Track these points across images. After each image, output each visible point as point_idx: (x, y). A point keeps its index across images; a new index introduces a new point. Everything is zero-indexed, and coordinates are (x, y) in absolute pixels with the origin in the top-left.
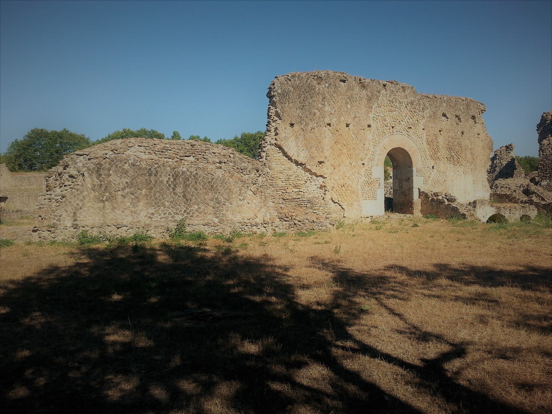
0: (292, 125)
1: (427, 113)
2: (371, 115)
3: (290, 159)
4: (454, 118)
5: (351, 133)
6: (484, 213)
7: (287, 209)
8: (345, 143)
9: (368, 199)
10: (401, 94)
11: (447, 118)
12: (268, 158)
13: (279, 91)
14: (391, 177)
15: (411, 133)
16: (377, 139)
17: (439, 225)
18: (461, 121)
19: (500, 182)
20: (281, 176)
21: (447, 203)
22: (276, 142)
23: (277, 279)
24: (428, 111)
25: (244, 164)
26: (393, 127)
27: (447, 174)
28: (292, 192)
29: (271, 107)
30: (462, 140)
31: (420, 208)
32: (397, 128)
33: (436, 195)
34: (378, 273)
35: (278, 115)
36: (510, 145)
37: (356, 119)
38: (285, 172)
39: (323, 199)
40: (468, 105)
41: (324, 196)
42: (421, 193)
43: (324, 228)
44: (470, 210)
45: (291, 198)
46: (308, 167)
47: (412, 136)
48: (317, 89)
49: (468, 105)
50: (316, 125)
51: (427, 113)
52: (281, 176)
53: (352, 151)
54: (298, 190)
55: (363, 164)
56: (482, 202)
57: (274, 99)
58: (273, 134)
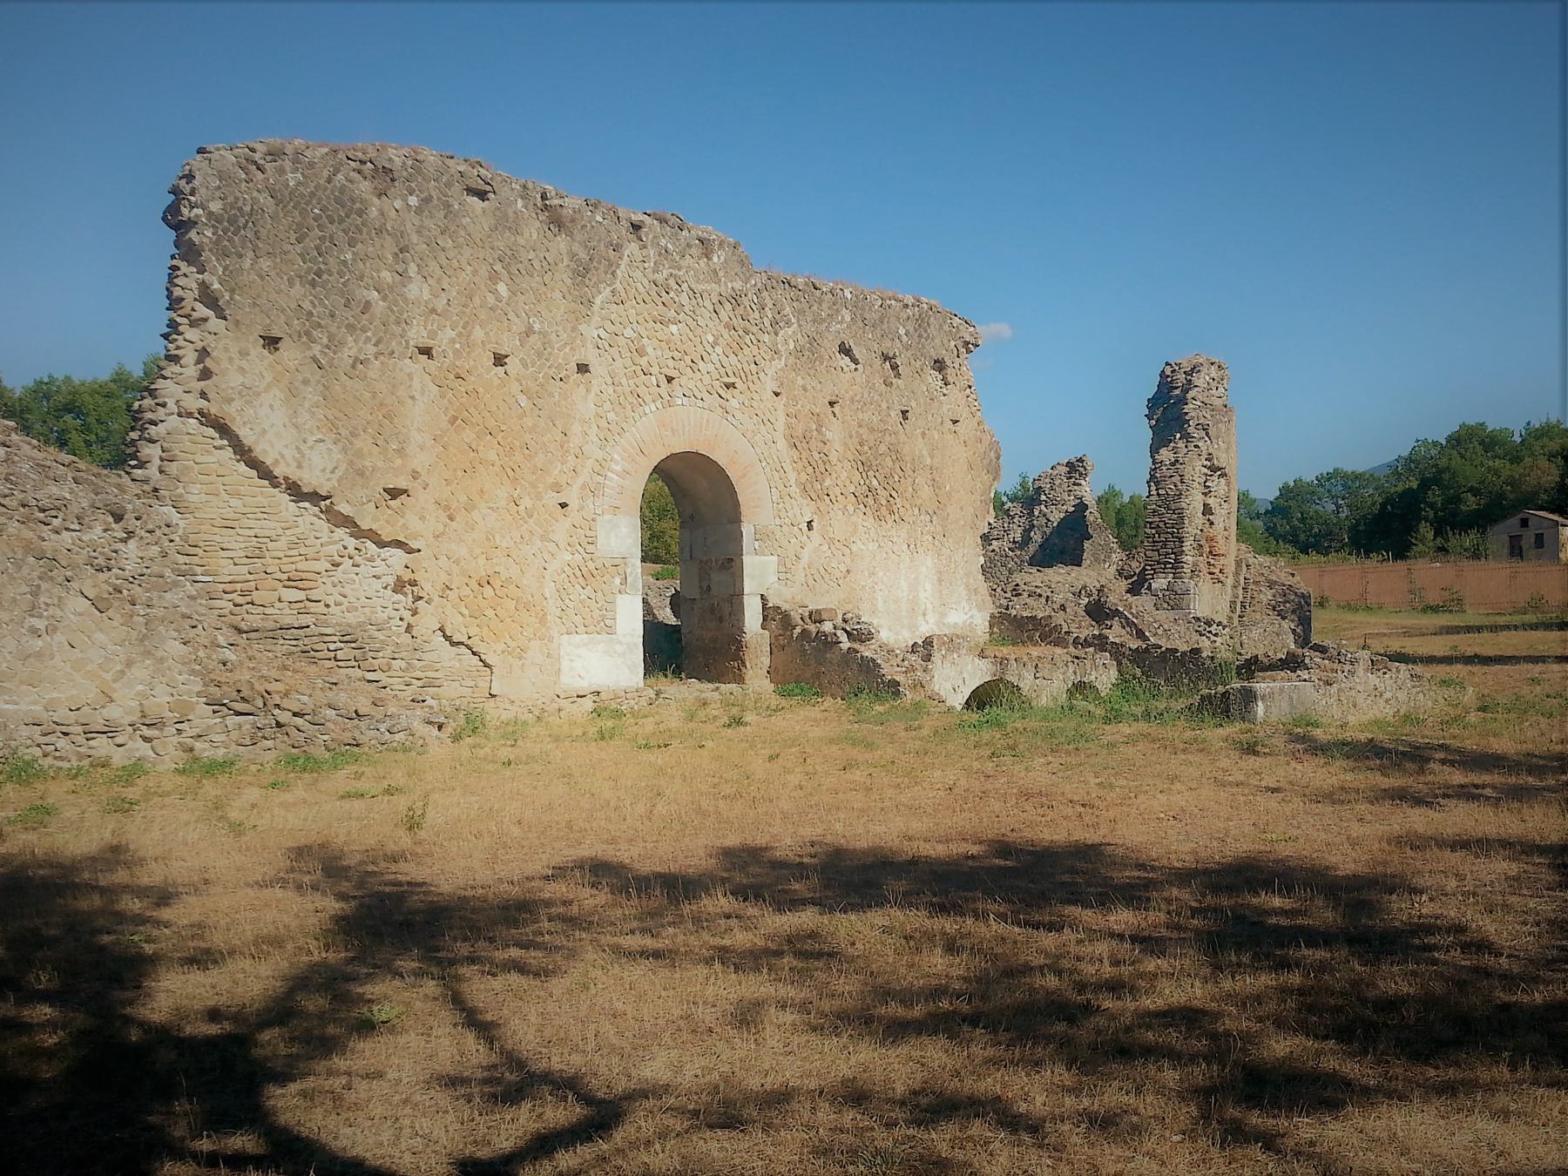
0: (272, 342)
1: (789, 336)
2: (590, 331)
3: (265, 474)
4: (878, 362)
5: (515, 388)
6: (955, 679)
7: (254, 667)
8: (491, 423)
9: (581, 629)
10: (694, 263)
11: (856, 361)
12: (173, 468)
13: (215, 206)
14: (1524, 523)
15: (734, 403)
16: (611, 416)
17: (816, 720)
18: (898, 375)
19: (1027, 578)
20: (225, 538)
21: (846, 644)
22: (202, 403)
23: (106, 939)
24: (790, 331)
25: (54, 490)
26: (670, 380)
27: (854, 548)
28: (280, 604)
29: (183, 265)
30: (903, 438)
31: (767, 661)
32: (686, 381)
33: (816, 617)
34: (515, 891)
35: (208, 298)
36: (1081, 460)
37: (533, 338)
38: (246, 522)
39: (409, 629)
40: (921, 323)
41: (412, 620)
42: (770, 613)
43: (400, 737)
44: (912, 669)
45: (270, 624)
46: (344, 508)
47: (738, 415)
48: (373, 212)
49: (921, 323)
50: (371, 349)
51: (789, 336)
52: (225, 538)
53: (518, 457)
54: (301, 595)
55: (563, 505)
56: (952, 642)
57: (193, 235)
58: (191, 370)
